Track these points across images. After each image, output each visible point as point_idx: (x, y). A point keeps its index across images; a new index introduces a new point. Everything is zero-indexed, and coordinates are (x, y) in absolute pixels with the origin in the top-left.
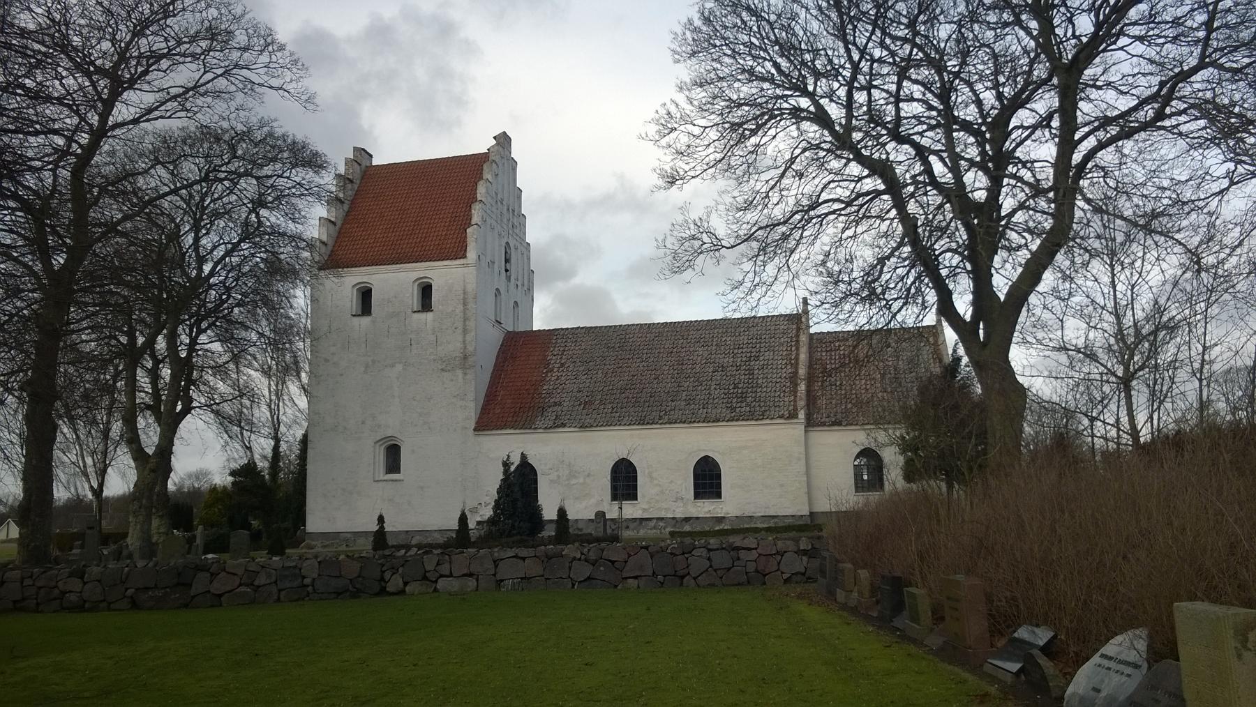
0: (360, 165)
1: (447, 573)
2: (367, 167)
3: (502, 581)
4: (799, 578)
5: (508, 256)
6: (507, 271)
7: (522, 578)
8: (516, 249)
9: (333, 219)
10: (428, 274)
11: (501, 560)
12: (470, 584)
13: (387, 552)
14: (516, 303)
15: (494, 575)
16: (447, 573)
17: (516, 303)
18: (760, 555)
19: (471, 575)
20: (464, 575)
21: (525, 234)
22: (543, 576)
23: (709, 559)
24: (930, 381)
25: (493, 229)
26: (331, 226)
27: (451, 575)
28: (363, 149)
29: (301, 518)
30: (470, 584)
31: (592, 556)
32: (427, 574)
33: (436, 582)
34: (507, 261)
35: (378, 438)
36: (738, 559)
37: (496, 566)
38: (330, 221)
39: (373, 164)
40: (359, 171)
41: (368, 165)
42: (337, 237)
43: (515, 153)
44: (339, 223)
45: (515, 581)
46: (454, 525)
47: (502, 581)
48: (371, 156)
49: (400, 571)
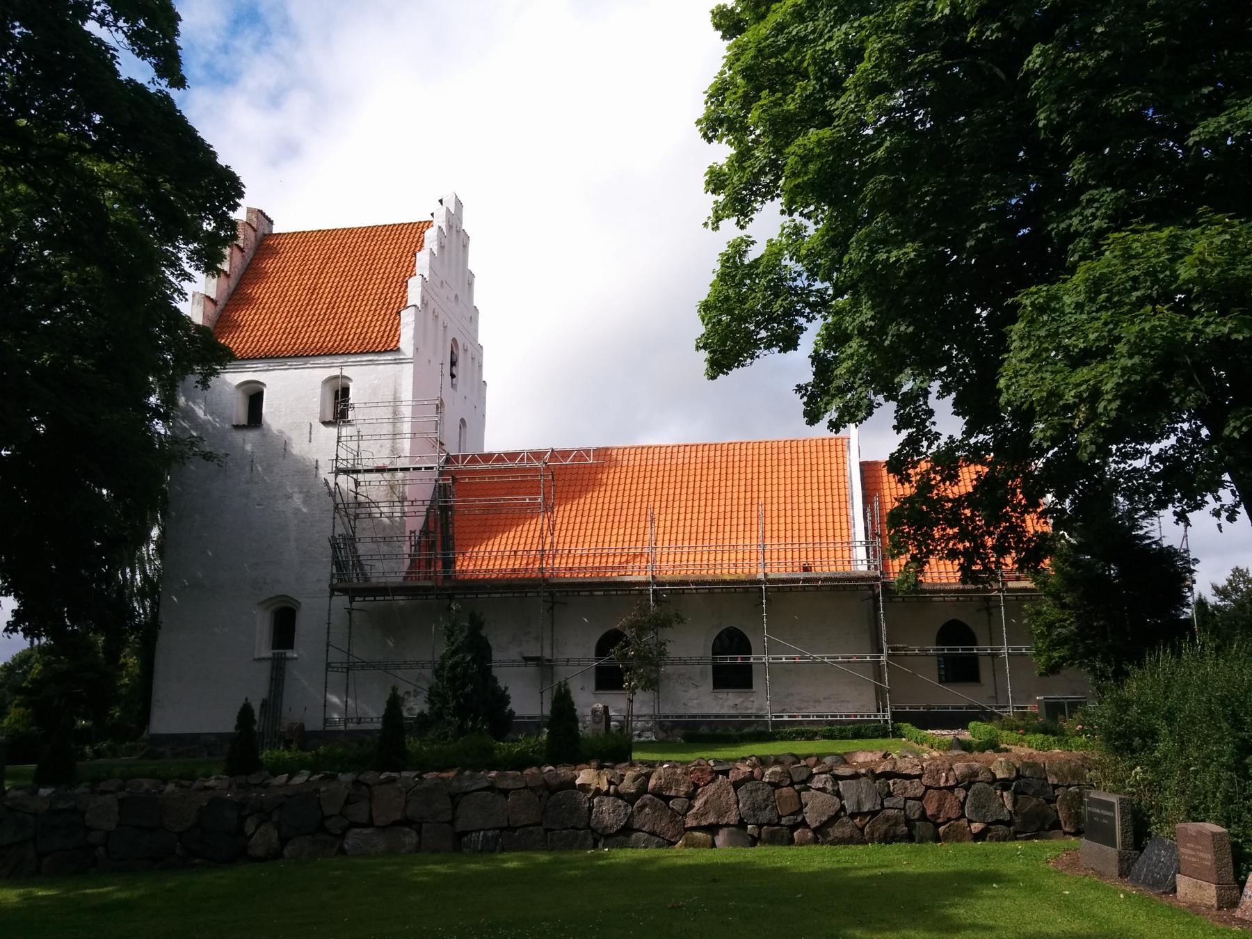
0: (255, 231)
1: (363, 818)
2: (265, 235)
3: (465, 833)
4: (1001, 829)
5: (454, 357)
6: (453, 376)
7: (502, 829)
8: (466, 350)
9: (213, 296)
10: (347, 372)
11: (466, 793)
12: (407, 840)
13: (254, 779)
14: (463, 421)
15: (452, 823)
16: (363, 818)
17: (463, 421)
18: (928, 788)
19: (406, 822)
20: (396, 823)
21: (476, 331)
22: (540, 824)
23: (838, 794)
24: (941, 559)
25: (437, 317)
26: (210, 305)
27: (370, 824)
28: (261, 212)
29: (144, 717)
30: (407, 840)
31: (628, 786)
32: (328, 824)
33: (342, 836)
34: (453, 363)
35: (263, 599)
36: (890, 794)
37: (455, 806)
38: (208, 297)
39: (274, 232)
40: (253, 239)
41: (266, 232)
42: (218, 321)
43: (466, 226)
44: (221, 303)
45: (489, 834)
46: (228, 725)
47: (465, 833)
48: (271, 222)
49: (275, 818)
